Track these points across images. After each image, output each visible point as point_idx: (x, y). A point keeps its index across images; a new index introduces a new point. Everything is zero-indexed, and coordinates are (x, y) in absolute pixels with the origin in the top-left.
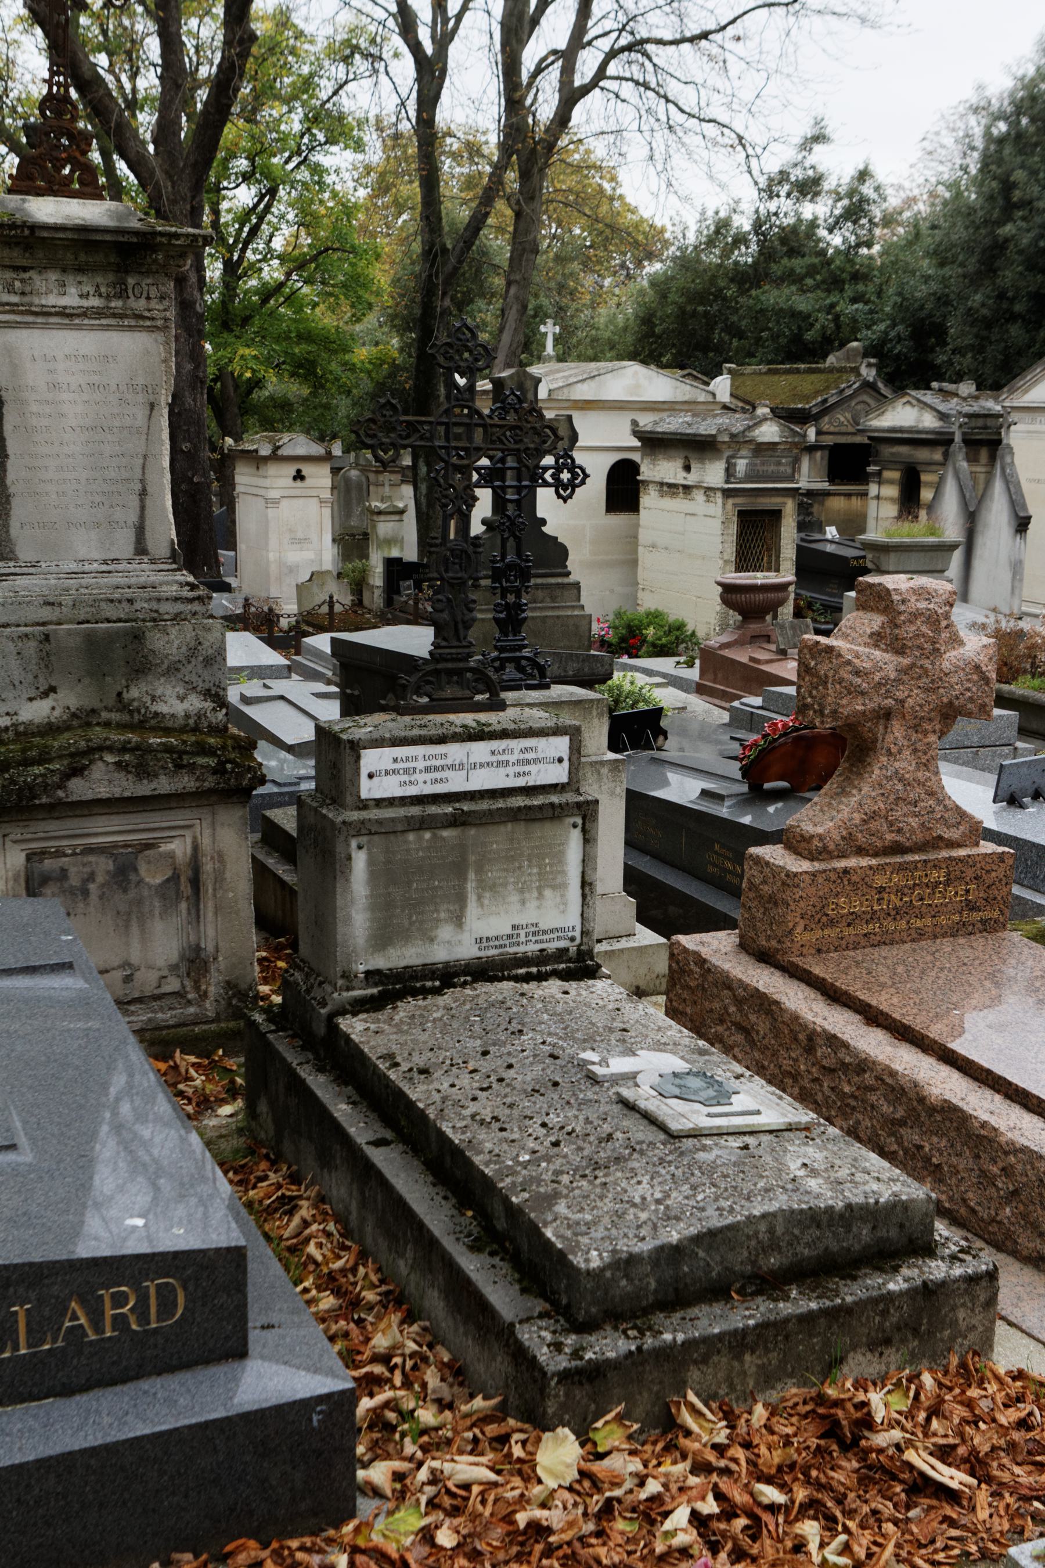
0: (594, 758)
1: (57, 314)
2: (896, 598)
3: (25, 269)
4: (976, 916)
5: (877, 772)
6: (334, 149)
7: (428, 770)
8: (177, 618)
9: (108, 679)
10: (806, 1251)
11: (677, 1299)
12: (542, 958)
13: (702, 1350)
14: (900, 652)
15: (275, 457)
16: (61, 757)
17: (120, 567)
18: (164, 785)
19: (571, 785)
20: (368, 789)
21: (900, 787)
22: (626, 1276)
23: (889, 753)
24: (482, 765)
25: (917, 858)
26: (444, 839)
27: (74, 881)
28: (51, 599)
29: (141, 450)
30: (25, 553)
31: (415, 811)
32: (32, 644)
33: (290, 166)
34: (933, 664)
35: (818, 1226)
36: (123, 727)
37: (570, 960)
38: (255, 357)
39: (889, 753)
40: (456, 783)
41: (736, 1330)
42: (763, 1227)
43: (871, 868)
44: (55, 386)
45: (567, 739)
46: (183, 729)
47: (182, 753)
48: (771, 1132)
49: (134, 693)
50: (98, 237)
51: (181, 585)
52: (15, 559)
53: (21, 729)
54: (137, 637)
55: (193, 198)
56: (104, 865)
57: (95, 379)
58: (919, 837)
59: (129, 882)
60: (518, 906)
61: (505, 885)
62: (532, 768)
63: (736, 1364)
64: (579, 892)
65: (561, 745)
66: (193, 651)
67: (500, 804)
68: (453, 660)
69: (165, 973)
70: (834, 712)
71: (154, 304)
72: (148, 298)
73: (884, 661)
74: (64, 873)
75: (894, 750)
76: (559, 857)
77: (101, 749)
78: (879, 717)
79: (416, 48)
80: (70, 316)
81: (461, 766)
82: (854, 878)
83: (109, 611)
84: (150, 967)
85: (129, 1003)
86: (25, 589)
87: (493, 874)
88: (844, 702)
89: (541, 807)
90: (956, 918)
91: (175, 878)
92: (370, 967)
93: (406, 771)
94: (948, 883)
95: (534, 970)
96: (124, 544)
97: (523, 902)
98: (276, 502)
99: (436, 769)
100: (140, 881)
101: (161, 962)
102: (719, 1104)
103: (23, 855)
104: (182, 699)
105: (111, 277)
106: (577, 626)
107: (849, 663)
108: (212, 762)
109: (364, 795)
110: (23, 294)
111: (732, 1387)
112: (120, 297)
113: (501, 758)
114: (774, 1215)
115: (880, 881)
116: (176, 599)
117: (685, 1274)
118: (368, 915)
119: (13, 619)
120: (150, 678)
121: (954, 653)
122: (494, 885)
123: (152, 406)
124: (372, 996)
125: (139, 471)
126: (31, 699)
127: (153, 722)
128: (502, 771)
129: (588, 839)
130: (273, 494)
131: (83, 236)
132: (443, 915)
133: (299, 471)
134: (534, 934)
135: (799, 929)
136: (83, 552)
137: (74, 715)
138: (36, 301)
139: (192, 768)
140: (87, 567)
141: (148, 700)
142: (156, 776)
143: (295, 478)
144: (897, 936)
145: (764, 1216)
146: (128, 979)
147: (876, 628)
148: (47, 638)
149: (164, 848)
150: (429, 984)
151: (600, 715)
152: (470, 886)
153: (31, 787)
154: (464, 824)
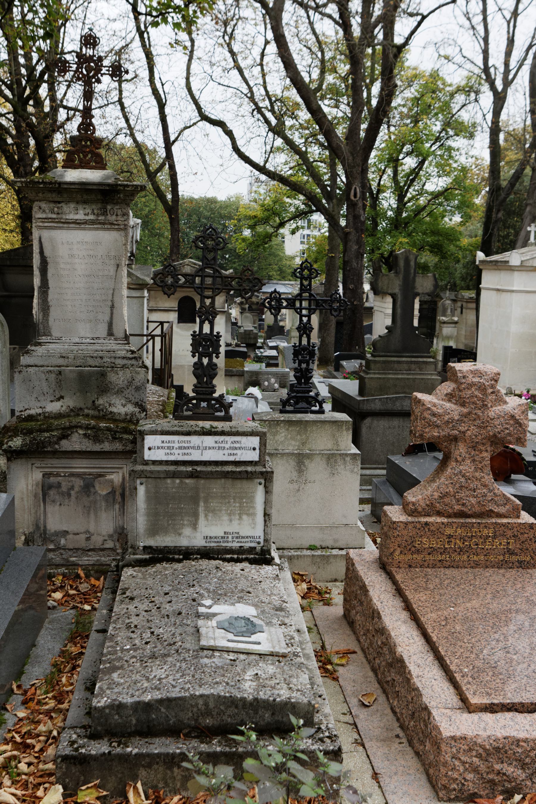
0: (342, 452)
1: (73, 223)
2: (459, 375)
3: (59, 202)
4: (514, 558)
5: (449, 470)
6: (457, 138)
7: (180, 448)
8: (124, 367)
9: (88, 394)
10: (229, 720)
11: (148, 731)
12: (241, 551)
13: (151, 760)
14: (463, 405)
16: (57, 429)
17: (100, 341)
18: (107, 446)
19: (261, 462)
20: (148, 455)
21: (463, 480)
22: (118, 714)
23: (457, 461)
24: (210, 448)
25: (474, 521)
26: (186, 484)
27: (64, 489)
29: (112, 287)
30: (55, 333)
31: (172, 468)
32: (53, 375)
33: (433, 148)
34: (483, 413)
35: (236, 707)
36: (93, 417)
38: (408, 243)
39: (457, 461)
40: (196, 456)
41: (168, 754)
42: (201, 702)
43: (443, 523)
44: (72, 256)
45: (258, 438)
46: (124, 421)
47: (116, 432)
48: (260, 655)
49: (101, 401)
50: (90, 187)
51: (127, 351)
52: (51, 335)
54: (103, 375)
55: (363, 164)
56: (78, 483)
57: (91, 253)
58: (477, 509)
59: (90, 492)
60: (228, 522)
61: (220, 511)
62: (239, 452)
63: (169, 772)
64: (263, 519)
65: (255, 441)
66: (130, 383)
67: (219, 469)
68: (204, 394)
69: (106, 538)
70: (421, 436)
71: (119, 218)
72: (117, 215)
73: (453, 410)
74: (59, 485)
75: (459, 459)
76: (252, 499)
77: (76, 427)
78: (452, 440)
79: (493, 87)
80: (78, 223)
82: (432, 528)
83: (91, 362)
84: (99, 534)
85: (89, 550)
86: (53, 349)
87: (213, 504)
88: (427, 430)
89: (240, 472)
90: (501, 558)
91: (113, 492)
93: (169, 448)
94: (495, 537)
95: (236, 556)
96: (102, 330)
97: (231, 521)
99: (185, 448)
100: (96, 492)
101: (104, 533)
102: (243, 636)
103: (41, 474)
104: (124, 406)
105: (99, 206)
107: (429, 409)
108: (131, 437)
109: (146, 458)
110: (58, 214)
111: (166, 784)
112: (103, 214)
113: (220, 445)
114: (208, 696)
115: (448, 531)
116: (124, 358)
117: (153, 719)
118: (145, 518)
119: (46, 363)
120: (108, 395)
121: (499, 407)
122: (214, 510)
123: (118, 266)
124: (146, 559)
125: (111, 296)
126: (52, 401)
127: (110, 416)
128: (221, 452)
129: (268, 491)
131: (83, 187)
132: (186, 522)
134: (237, 538)
135: (397, 552)
137: (72, 410)
138: (64, 217)
139: (121, 439)
140: (84, 341)
141: (107, 405)
142: (103, 442)
144: (461, 564)
145: (201, 696)
146: (88, 539)
147: (449, 391)
148: (60, 373)
149: (108, 477)
150: (177, 557)
151: (347, 430)
152: (201, 509)
153: (43, 442)
154: (197, 477)
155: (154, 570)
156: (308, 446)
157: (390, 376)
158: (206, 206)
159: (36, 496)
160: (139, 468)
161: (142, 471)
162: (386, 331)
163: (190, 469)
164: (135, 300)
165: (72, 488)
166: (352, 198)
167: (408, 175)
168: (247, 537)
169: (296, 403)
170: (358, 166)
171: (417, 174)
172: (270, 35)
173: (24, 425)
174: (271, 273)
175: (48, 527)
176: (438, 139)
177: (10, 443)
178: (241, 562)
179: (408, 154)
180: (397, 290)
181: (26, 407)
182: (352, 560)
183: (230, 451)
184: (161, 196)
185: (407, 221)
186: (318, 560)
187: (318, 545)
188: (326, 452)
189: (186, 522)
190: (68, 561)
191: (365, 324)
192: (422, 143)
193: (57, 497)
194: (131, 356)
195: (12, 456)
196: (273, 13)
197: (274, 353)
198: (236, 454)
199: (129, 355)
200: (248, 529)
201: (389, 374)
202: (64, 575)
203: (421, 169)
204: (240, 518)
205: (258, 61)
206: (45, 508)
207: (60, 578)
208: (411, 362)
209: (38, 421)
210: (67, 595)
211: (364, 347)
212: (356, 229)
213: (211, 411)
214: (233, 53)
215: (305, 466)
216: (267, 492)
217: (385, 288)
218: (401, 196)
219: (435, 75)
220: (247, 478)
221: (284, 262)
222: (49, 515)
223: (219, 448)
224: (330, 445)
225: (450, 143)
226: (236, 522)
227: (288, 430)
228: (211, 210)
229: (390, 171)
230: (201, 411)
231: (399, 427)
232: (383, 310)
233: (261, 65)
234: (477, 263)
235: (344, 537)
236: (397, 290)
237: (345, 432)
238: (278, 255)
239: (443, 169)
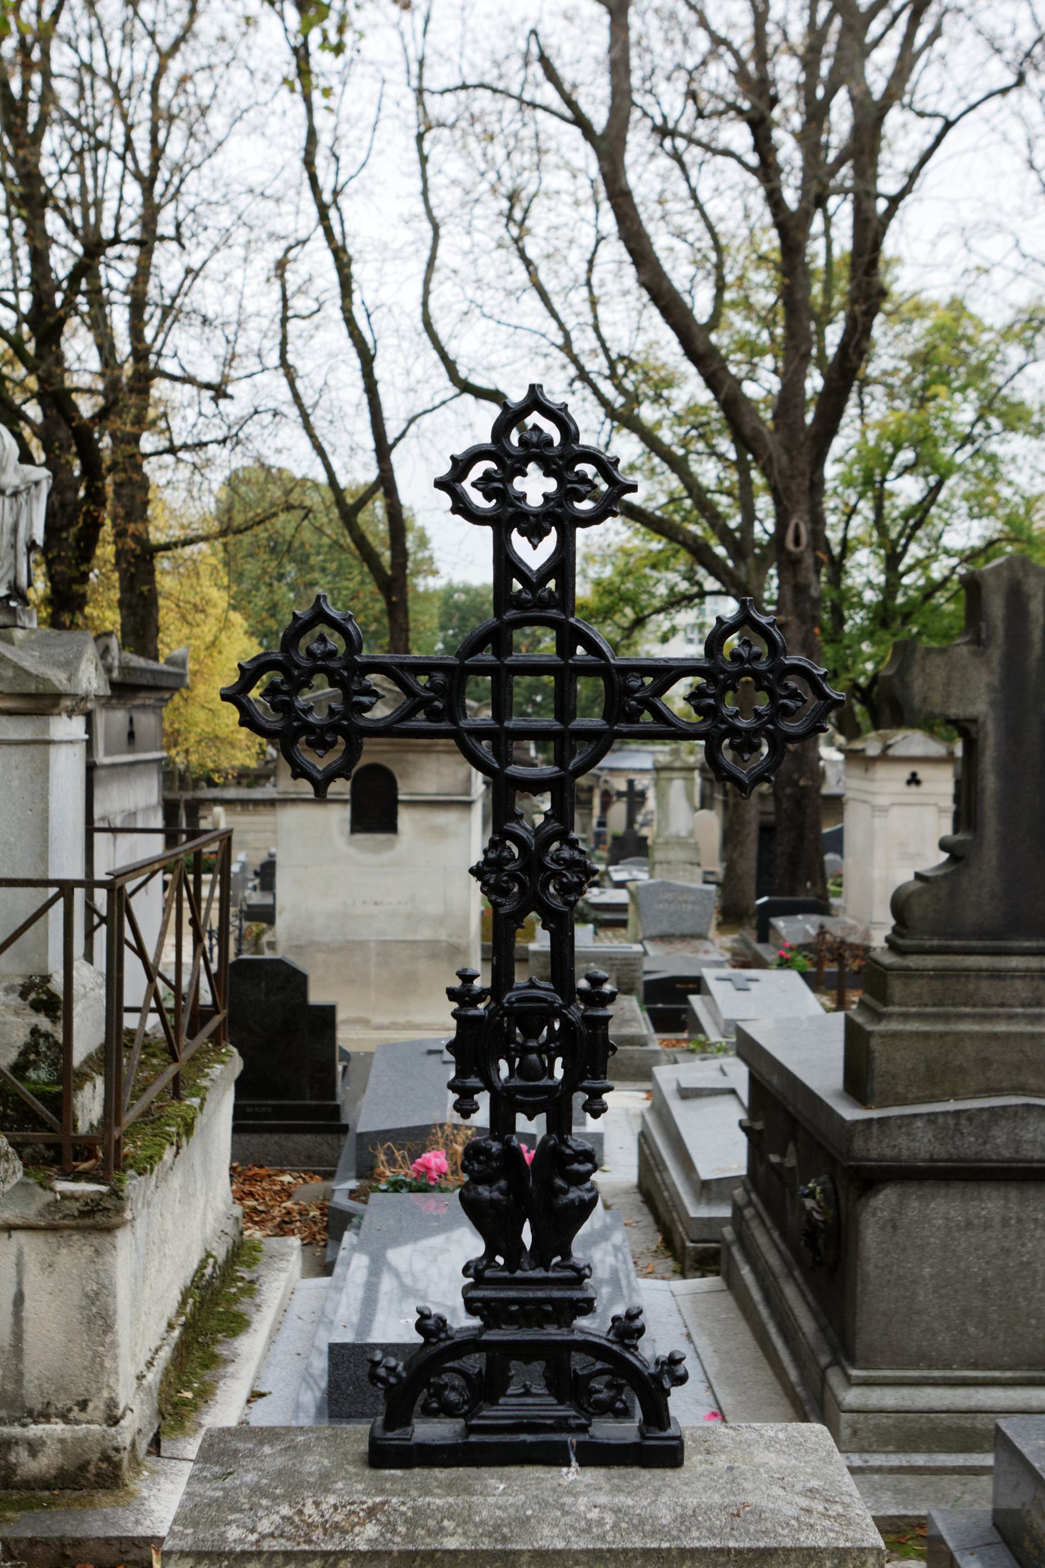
6: (1010, 436)
15: (885, 757)
55: (813, 473)
98: (885, 810)
130: (882, 801)
133: (914, 775)
143: (909, 782)
162: (944, 856)
164: (17, 754)
166: (790, 545)
167: (906, 517)
170: (802, 475)
171: (927, 511)
172: (609, 222)
176: (968, 439)
179: (907, 469)
180: (979, 705)
184: (368, 555)
185: (906, 610)
191: (826, 830)
192: (935, 445)
196: (604, 146)
197: (620, 896)
201: (961, 1017)
203: (933, 501)
205: (583, 278)
211: (824, 882)
212: (801, 617)
214: (528, 263)
217: (936, 698)
218: (892, 561)
219: (957, 307)
225: (993, 446)
229: (866, 508)
231: (1005, 1222)
232: (868, 797)
233: (588, 283)
236: (979, 705)
239: (980, 506)
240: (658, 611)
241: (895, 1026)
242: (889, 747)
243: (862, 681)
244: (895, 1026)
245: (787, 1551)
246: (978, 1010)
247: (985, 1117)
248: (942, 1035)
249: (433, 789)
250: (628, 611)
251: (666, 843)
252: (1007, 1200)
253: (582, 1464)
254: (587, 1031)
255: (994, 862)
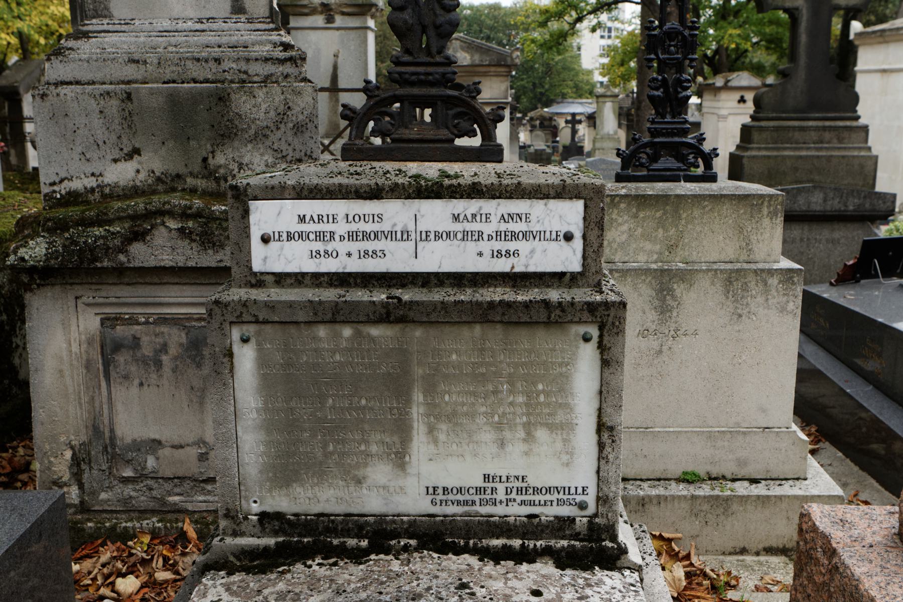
0: (760, 266)
7: (352, 236)
8: (267, 80)
12: (531, 527)
15: (726, 87)
16: (120, 219)
17: (215, 26)
19: (589, 274)
20: (263, 259)
24: (438, 236)
26: (372, 339)
27: (147, 350)
28: (136, 57)
31: (330, 295)
32: (115, 102)
37: (576, 536)
38: (739, 35)
40: (398, 259)
45: (579, 205)
49: (220, 159)
51: (275, 45)
52: (110, 16)
53: (107, 191)
54: (222, 99)
56: (176, 338)
60: (494, 449)
61: (472, 415)
64: (594, 438)
65: (570, 214)
67: (466, 295)
76: (561, 384)
77: (161, 213)
81: (405, 235)
83: (195, 71)
86: (113, 45)
87: (450, 398)
89: (527, 305)
92: (268, 509)
95: (517, 543)
97: (502, 444)
99: (366, 236)
103: (98, 319)
106: (862, 167)
113: (469, 227)
116: (266, 60)
118: (262, 436)
119: (98, 76)
120: (236, 143)
122: (454, 413)
124: (266, 549)
126: (115, 161)
128: (472, 247)
129: (608, 361)
130: (724, 112)
132: (374, 448)
133: (742, 97)
134: (519, 491)
136: (177, 11)
137: (159, 179)
140: (181, 25)
141: (235, 167)
143: (739, 102)
146: (203, 457)
150: (352, 542)
151: (773, 215)
152: (417, 412)
154: (402, 320)
155: (281, 586)
156: (681, 253)
157: (786, 153)
158: (488, 13)
159: (88, 366)
160: (237, 294)
161: (245, 304)
163: (381, 296)
164: (353, 34)
165: (164, 348)
168: (549, 490)
169: (654, 159)
173: (61, 213)
174: (565, 91)
175: (119, 433)
177: (22, 252)
178: (531, 561)
181: (63, 175)
182: (826, 538)
183: (497, 245)
185: (737, 8)
186: (706, 507)
187: (702, 471)
188: (723, 266)
189: (374, 448)
190: (163, 502)
193: (133, 368)
194: (282, 55)
195: (32, 279)
198: (516, 253)
199: (279, 54)
200: (558, 469)
201: (785, 149)
202: (154, 534)
204: (529, 437)
206: (110, 393)
207: (146, 539)
208: (824, 128)
209: (88, 202)
210: (151, 583)
213: (444, 133)
215: (674, 297)
216: (605, 363)
220: (548, 323)
221: (581, 77)
222: (119, 407)
223: (466, 236)
224: (730, 250)
226: (516, 448)
227: (635, 216)
228: (495, 17)
230: (413, 132)
231: (802, 240)
232: (716, 111)
234: (852, 37)
235: (761, 455)
237: (766, 221)
238: (574, 69)
240: (590, 13)
241: (754, 153)
242: (729, 81)
243: (709, 52)
244: (754, 153)
245: (754, 195)
246: (794, 145)
247: (795, 191)
248: (776, 157)
249: (488, 96)
250: (574, 13)
251: (602, 138)
252: (803, 230)
253: (685, 181)
254: (690, 39)
255: (803, 77)
